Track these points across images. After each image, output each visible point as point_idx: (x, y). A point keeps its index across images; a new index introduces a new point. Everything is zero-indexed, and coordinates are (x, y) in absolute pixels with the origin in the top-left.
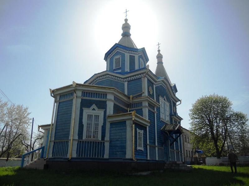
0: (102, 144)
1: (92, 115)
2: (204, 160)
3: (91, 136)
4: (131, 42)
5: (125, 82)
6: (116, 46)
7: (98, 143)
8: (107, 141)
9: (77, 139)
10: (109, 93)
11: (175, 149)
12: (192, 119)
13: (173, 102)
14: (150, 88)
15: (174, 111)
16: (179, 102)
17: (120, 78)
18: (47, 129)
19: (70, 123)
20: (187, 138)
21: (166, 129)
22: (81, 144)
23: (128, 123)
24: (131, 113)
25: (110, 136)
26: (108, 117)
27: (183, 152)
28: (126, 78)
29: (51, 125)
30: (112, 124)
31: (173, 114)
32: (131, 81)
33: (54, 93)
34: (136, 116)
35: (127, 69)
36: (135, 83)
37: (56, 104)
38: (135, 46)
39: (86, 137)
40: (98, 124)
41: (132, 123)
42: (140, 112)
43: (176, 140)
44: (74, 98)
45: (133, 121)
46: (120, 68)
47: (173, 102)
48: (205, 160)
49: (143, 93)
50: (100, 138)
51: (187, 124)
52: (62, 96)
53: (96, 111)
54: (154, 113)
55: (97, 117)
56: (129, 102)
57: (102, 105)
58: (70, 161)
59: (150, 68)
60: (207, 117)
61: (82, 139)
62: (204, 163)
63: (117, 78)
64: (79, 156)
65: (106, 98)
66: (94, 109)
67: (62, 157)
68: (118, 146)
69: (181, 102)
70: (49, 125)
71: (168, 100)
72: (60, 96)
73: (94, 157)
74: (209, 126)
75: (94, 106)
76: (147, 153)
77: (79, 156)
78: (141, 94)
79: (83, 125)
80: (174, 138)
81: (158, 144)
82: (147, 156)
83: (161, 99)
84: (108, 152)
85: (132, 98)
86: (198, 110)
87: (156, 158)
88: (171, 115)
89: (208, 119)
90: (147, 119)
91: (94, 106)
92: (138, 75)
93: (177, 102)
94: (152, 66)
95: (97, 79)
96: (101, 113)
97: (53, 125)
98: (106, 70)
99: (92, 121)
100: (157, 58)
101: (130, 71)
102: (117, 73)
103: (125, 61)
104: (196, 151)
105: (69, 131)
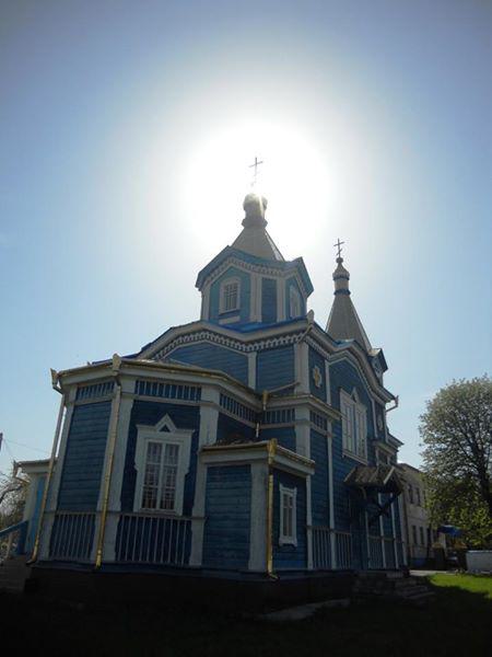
0: (185, 524)
1: (161, 445)
2: (462, 554)
3: (155, 501)
4: (265, 243)
5: (251, 352)
6: (227, 255)
7: (175, 521)
8: (198, 518)
9: (119, 509)
10: (209, 385)
11: (382, 534)
12: (426, 441)
13: (377, 402)
14: (317, 370)
15: (378, 427)
16: (393, 403)
17: (236, 341)
18: (38, 474)
19: (101, 464)
20: (415, 491)
21: (357, 480)
22: (127, 522)
23: (256, 470)
24: (265, 445)
25: (207, 504)
26: (204, 450)
27: (403, 539)
28: (252, 342)
29: (51, 463)
30: (212, 470)
31: (397, 566)
32: (266, 350)
33: (62, 380)
34: (277, 451)
35: (256, 316)
36: (276, 357)
37: (65, 409)
38: (276, 252)
39: (143, 505)
40: (176, 468)
41: (267, 470)
42: (287, 439)
43: (384, 510)
44: (114, 397)
45: (270, 466)
46: (238, 311)
47: (376, 402)
48: (464, 557)
49: (298, 384)
50: (179, 509)
51: (413, 452)
52: (84, 390)
53: (172, 434)
54: (326, 437)
55: (173, 450)
56: (260, 406)
57: (187, 418)
58: (103, 573)
59: (317, 319)
60: (467, 438)
61: (132, 510)
62: (461, 565)
63: (228, 341)
64: (123, 556)
65: (199, 398)
66: (165, 429)
67: (76, 558)
68: (228, 536)
69: (397, 403)
70: (46, 463)
71: (364, 399)
72: (79, 389)
73: (162, 561)
74: (475, 463)
75: (166, 421)
76: (306, 552)
77: (123, 556)
78: (292, 388)
79: (135, 472)
80: (380, 502)
81: (336, 523)
82: (306, 559)
83: (344, 397)
84: (201, 551)
85: (270, 397)
86: (442, 417)
87: (330, 564)
88: (371, 439)
89: (470, 445)
90: (307, 458)
91: (166, 421)
92: (284, 335)
93: (385, 402)
94: (320, 306)
95: (174, 343)
96: (183, 439)
97: (55, 462)
98: (199, 319)
99: (159, 461)
100: (335, 279)
101: (263, 319)
102: (224, 327)
103: (249, 292)
104: (442, 530)
105: (99, 487)
